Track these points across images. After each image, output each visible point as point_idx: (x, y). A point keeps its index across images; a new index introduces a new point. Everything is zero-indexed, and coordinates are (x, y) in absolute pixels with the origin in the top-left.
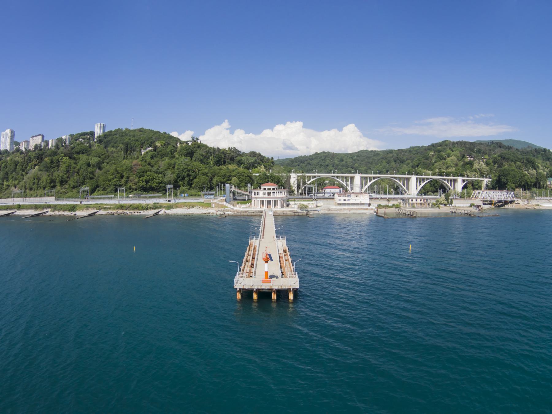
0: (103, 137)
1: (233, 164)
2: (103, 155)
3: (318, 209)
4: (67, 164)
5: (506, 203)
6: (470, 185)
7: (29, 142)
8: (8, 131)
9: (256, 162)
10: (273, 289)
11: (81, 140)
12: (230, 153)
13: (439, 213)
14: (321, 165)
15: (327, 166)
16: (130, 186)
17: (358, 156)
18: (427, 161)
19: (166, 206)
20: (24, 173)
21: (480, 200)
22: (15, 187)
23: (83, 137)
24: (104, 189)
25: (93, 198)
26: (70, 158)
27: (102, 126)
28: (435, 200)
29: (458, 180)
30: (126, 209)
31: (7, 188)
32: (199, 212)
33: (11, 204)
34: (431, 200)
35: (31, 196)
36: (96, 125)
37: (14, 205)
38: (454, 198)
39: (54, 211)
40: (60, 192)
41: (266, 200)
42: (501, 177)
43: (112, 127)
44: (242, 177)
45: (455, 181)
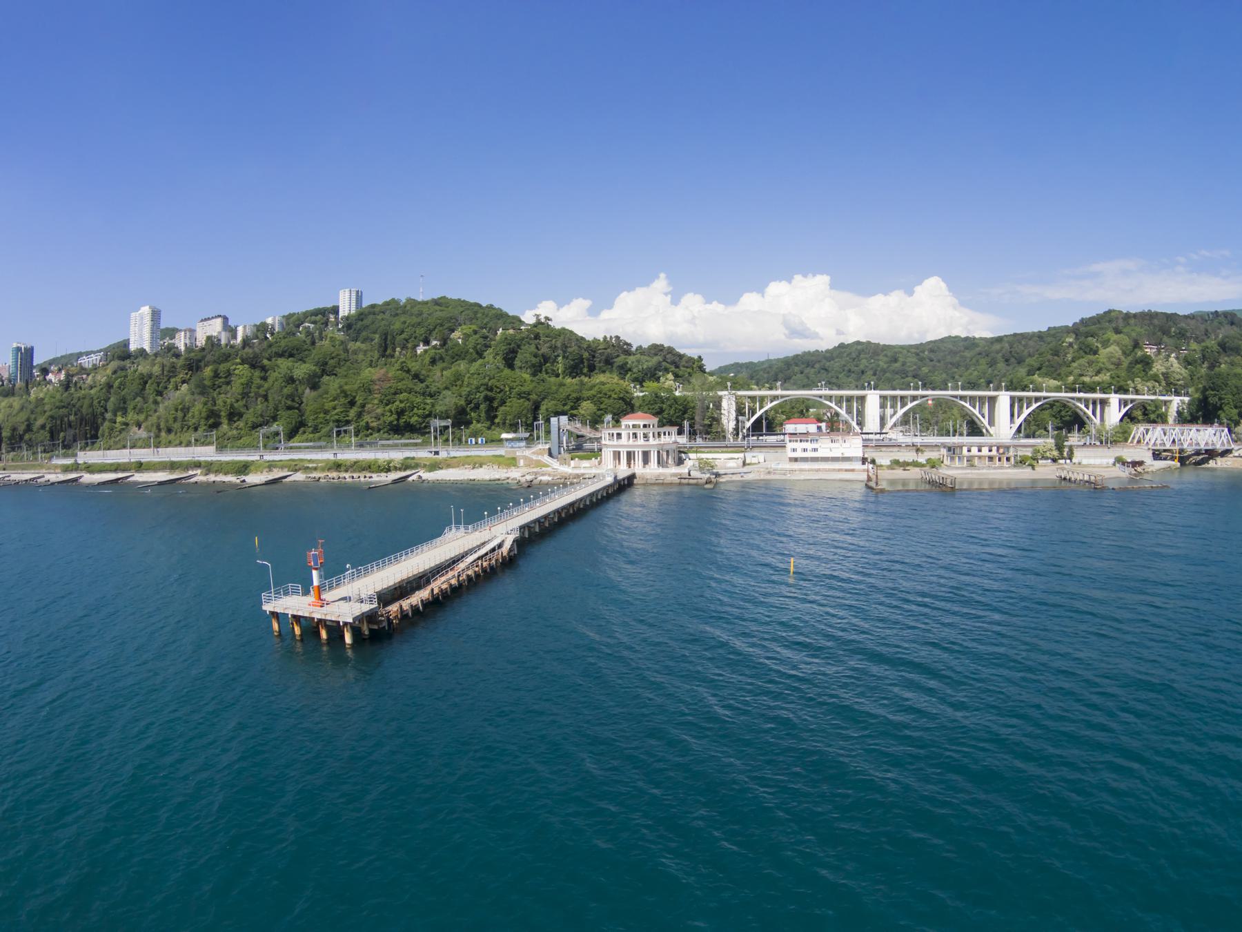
0: (354, 319)
1: (611, 372)
2: (333, 358)
3: (746, 469)
4: (243, 380)
5: (1211, 454)
6: (1138, 414)
7: (195, 331)
8: (146, 310)
9: (658, 367)
10: (314, 618)
11: (307, 324)
12: (605, 349)
13: (1034, 481)
14: (849, 371)
15: (863, 372)
16: (367, 423)
17: (932, 351)
18: (1056, 357)
19: (428, 464)
20: (159, 398)
21: (1146, 448)
22: (139, 426)
23: (313, 318)
24: (316, 430)
25: (291, 448)
26: (253, 366)
27: (354, 295)
28: (1031, 449)
29: (1111, 400)
30: (346, 471)
31: (123, 429)
32: (487, 477)
33: (126, 460)
34: (1019, 449)
35: (169, 444)
36: (341, 293)
37: (130, 463)
38: (1088, 444)
39: (207, 474)
40: (226, 437)
41: (626, 450)
42: (1207, 393)
43: (377, 297)
44: (606, 401)
45: (1104, 403)
